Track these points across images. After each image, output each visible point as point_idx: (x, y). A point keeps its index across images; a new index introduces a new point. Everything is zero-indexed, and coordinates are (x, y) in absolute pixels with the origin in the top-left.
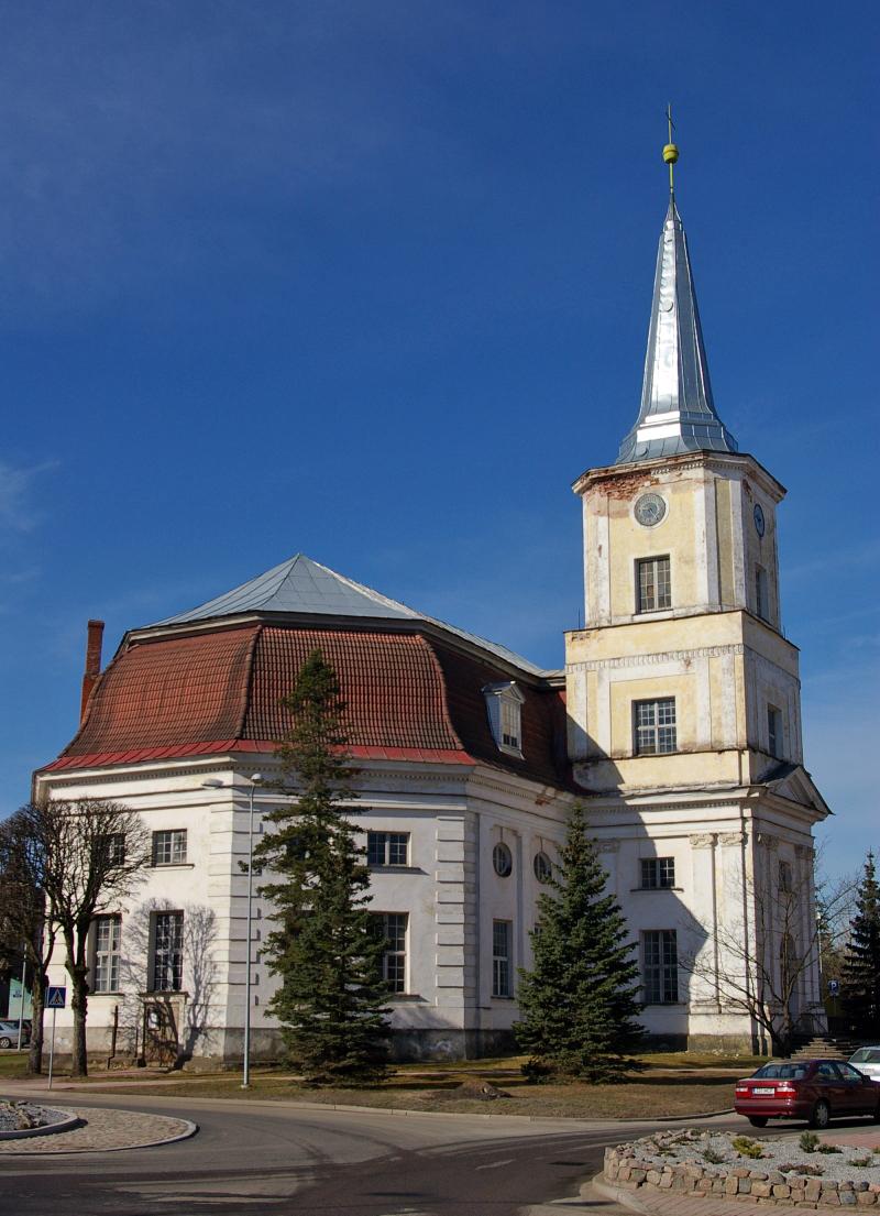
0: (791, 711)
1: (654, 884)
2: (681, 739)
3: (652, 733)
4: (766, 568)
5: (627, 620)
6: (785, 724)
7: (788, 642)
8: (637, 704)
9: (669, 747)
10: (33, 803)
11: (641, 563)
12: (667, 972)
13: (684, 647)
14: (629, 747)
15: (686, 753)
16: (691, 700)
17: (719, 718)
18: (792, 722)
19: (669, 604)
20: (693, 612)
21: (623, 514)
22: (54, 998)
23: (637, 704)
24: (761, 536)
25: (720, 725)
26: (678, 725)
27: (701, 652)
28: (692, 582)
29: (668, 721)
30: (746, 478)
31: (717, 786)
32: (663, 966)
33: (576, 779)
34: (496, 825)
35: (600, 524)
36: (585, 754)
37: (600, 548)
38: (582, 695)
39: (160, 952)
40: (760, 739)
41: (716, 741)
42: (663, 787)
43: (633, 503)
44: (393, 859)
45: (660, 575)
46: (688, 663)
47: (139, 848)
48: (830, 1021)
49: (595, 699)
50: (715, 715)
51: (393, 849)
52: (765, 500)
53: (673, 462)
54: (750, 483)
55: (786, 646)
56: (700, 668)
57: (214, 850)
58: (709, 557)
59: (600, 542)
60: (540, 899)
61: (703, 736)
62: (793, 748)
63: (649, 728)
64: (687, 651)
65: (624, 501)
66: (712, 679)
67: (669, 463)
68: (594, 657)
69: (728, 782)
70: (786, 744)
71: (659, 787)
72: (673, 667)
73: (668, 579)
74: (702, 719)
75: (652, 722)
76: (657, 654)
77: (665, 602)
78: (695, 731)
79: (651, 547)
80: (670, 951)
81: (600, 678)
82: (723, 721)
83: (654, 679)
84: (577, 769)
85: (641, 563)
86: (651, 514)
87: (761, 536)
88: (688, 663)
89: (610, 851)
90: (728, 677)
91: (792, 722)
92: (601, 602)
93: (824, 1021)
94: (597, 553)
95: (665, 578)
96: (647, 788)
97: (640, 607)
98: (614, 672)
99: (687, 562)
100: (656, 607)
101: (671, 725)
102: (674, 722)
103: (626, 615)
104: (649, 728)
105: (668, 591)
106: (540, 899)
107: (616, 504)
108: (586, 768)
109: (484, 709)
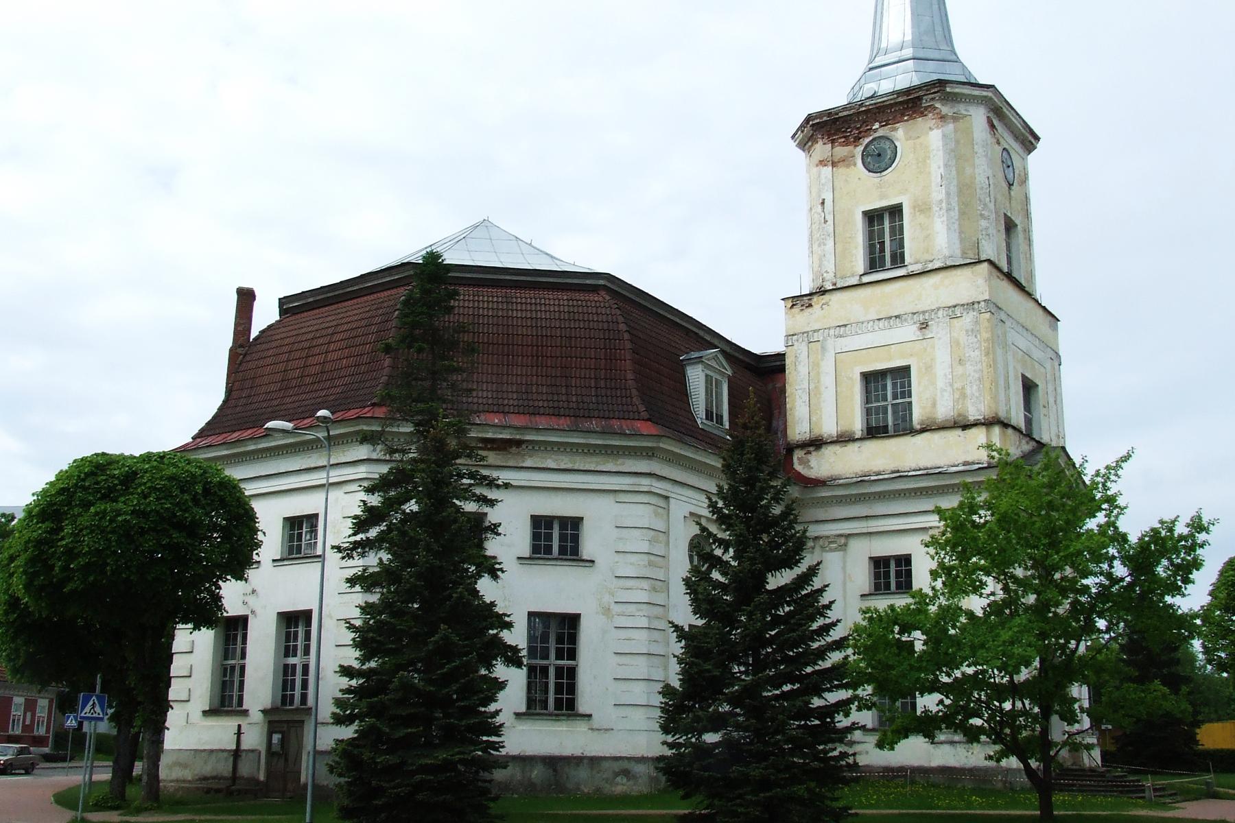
0: (1050, 388)
1: (888, 586)
2: (917, 416)
4: (1017, 222)
5: (855, 281)
6: (1042, 401)
7: (1044, 308)
9: (905, 428)
11: (872, 217)
12: (559, 670)
13: (920, 308)
14: (857, 425)
15: (923, 431)
16: (929, 368)
17: (963, 388)
18: (1051, 400)
19: (903, 260)
20: (930, 266)
21: (845, 161)
24: (1010, 185)
25: (963, 396)
26: (914, 399)
27: (940, 313)
28: (928, 236)
29: (903, 395)
30: (991, 115)
31: (961, 468)
32: (553, 661)
33: (798, 467)
34: (691, 514)
35: (823, 177)
36: (807, 436)
37: (823, 203)
38: (803, 369)
39: (292, 660)
40: (1013, 414)
41: (960, 415)
42: (898, 471)
43: (860, 149)
45: (892, 229)
46: (924, 326)
47: (271, 539)
48: (1104, 755)
49: (818, 373)
50: (957, 385)
51: (563, 538)
52: (1014, 146)
53: (905, 98)
54: (996, 122)
55: (1041, 312)
56: (939, 330)
57: (660, 609)
58: (949, 203)
60: (500, 530)
61: (944, 411)
62: (1054, 430)
64: (924, 312)
65: (850, 148)
66: (954, 344)
67: (900, 99)
69: (973, 463)
70: (1044, 425)
71: (893, 472)
72: (908, 331)
73: (902, 232)
74: (943, 390)
76: (890, 318)
77: (898, 259)
78: (934, 405)
79: (882, 197)
80: (823, 659)
81: (823, 349)
82: (968, 392)
83: (887, 346)
84: (798, 454)
85: (872, 217)
86: (879, 160)
87: (1010, 185)
88: (924, 326)
89: (835, 550)
90: (972, 339)
91: (1051, 400)
92: (825, 263)
93: (1096, 753)
95: (898, 231)
96: (878, 474)
97: (874, 263)
99: (921, 211)
100: (888, 265)
102: (910, 396)
103: (853, 275)
105: (902, 246)
107: (841, 151)
108: (809, 453)
109: (684, 375)
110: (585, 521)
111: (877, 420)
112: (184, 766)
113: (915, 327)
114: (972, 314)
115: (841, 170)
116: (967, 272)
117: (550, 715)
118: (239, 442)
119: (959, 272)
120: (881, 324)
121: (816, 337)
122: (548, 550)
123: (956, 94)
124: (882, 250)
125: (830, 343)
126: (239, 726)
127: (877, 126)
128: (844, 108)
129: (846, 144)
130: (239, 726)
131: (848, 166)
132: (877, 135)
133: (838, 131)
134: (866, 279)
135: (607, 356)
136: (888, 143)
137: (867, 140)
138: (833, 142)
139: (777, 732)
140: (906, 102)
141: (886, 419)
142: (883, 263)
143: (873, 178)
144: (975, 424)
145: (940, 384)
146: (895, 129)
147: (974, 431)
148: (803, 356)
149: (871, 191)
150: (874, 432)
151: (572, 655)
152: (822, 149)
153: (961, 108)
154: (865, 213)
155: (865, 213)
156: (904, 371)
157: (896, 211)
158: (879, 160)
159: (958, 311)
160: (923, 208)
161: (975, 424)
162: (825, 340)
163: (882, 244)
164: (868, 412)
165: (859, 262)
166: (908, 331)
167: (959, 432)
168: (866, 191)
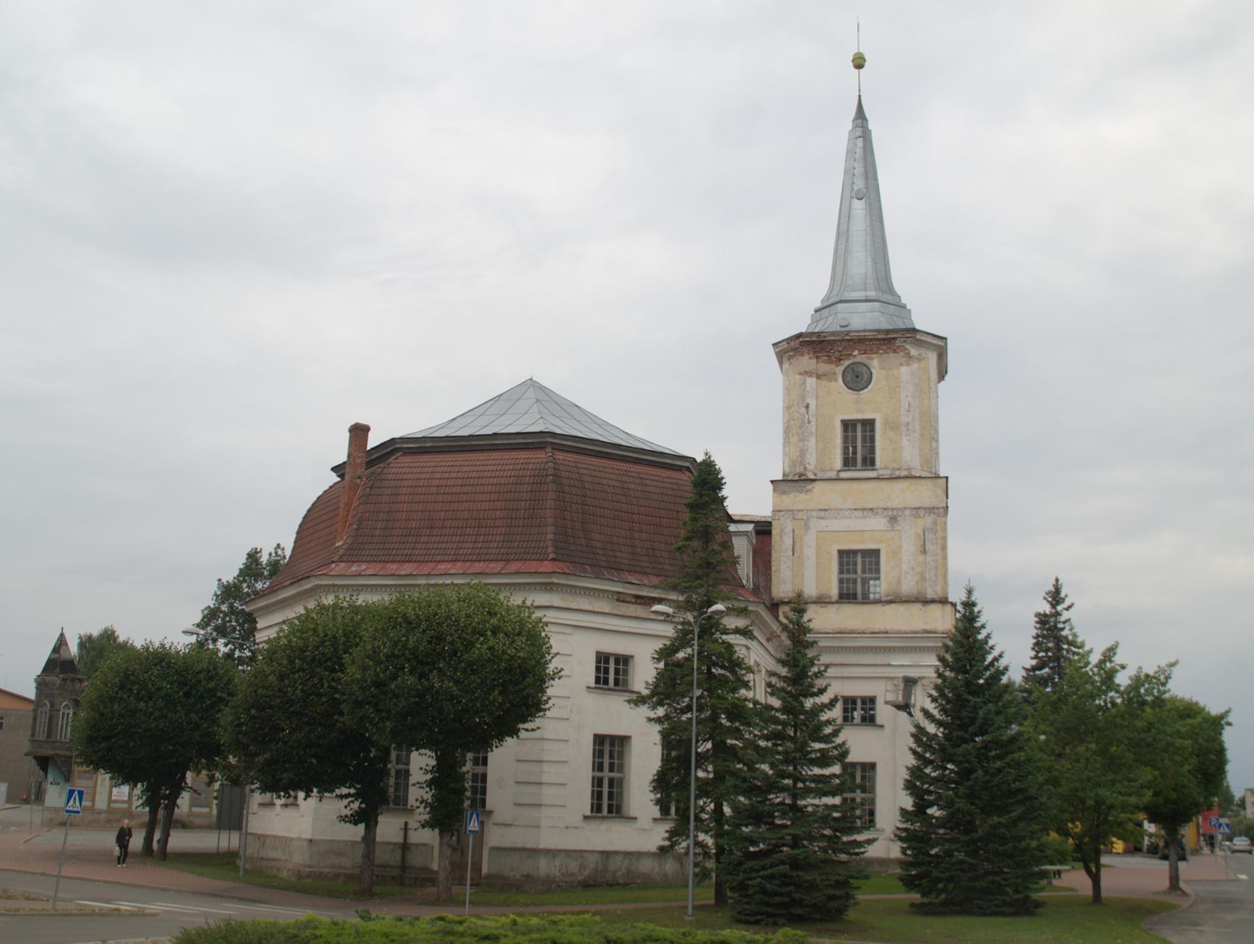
3: (855, 582)
5: (833, 475)
8: (842, 553)
10: (731, 520)
12: (611, 781)
13: (889, 505)
14: (834, 592)
20: (897, 473)
21: (830, 377)
22: (71, 802)
23: (842, 553)
27: (907, 512)
32: (606, 774)
35: (808, 385)
37: (807, 407)
43: (841, 368)
44: (617, 682)
45: (864, 438)
59: (808, 401)
63: (852, 576)
64: (893, 509)
65: (833, 366)
68: (800, 507)
72: (879, 523)
75: (855, 572)
76: (864, 510)
77: (869, 462)
78: (899, 582)
79: (858, 411)
81: (807, 527)
83: (865, 532)
86: (857, 380)
88: (893, 519)
94: (803, 410)
97: (848, 462)
98: (824, 523)
99: (891, 429)
101: (845, 576)
103: (831, 470)
104: (852, 576)
106: (913, 730)
107: (824, 367)
110: (636, 659)
111: (848, 588)
112: (340, 854)
113: (885, 520)
114: (933, 516)
115: (825, 383)
116: (929, 483)
117: (604, 818)
118: (358, 575)
119: (923, 481)
120: (856, 513)
121: (800, 515)
122: (606, 682)
123: (921, 341)
124: (855, 453)
125: (813, 523)
126: (406, 823)
127: (856, 353)
128: (833, 334)
129: (830, 362)
130: (406, 823)
131: (830, 380)
132: (856, 360)
133: (822, 350)
134: (843, 475)
135: (642, 515)
136: (865, 370)
137: (847, 363)
138: (818, 358)
139: (254, 717)
140: (884, 339)
141: (855, 588)
142: (855, 464)
143: (851, 395)
144: (933, 601)
145: (904, 567)
146: (872, 359)
147: (933, 606)
148: (789, 529)
149: (850, 405)
150: (847, 596)
151: (621, 769)
152: (807, 361)
153: (923, 352)
154: (842, 421)
155: (842, 421)
156: (876, 553)
157: (869, 424)
158: (857, 380)
159: (922, 512)
160: (893, 426)
161: (933, 601)
162: (808, 519)
163: (855, 448)
164: (841, 581)
165: (838, 463)
166: (879, 523)
167: (919, 606)
168: (845, 404)
